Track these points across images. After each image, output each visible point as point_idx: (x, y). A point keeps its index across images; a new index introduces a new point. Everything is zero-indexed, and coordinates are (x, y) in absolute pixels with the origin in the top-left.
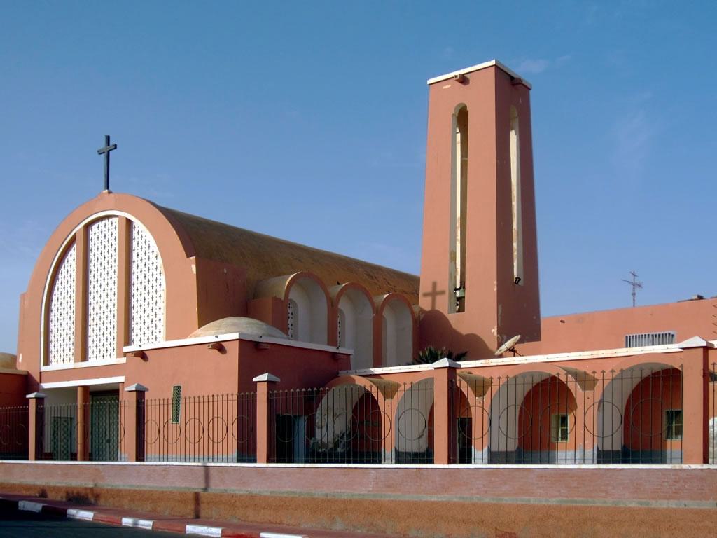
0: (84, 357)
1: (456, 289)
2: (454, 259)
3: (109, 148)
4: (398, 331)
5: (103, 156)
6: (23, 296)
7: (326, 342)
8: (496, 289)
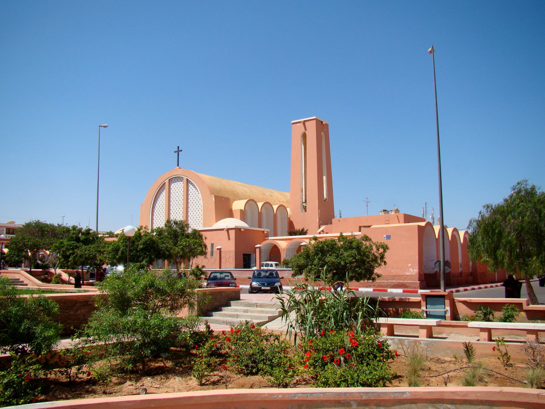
0: (220, 268)
1: (303, 203)
2: (302, 191)
3: (178, 151)
4: (282, 226)
5: (177, 153)
6: (142, 205)
7: (258, 226)
8: (317, 204)
